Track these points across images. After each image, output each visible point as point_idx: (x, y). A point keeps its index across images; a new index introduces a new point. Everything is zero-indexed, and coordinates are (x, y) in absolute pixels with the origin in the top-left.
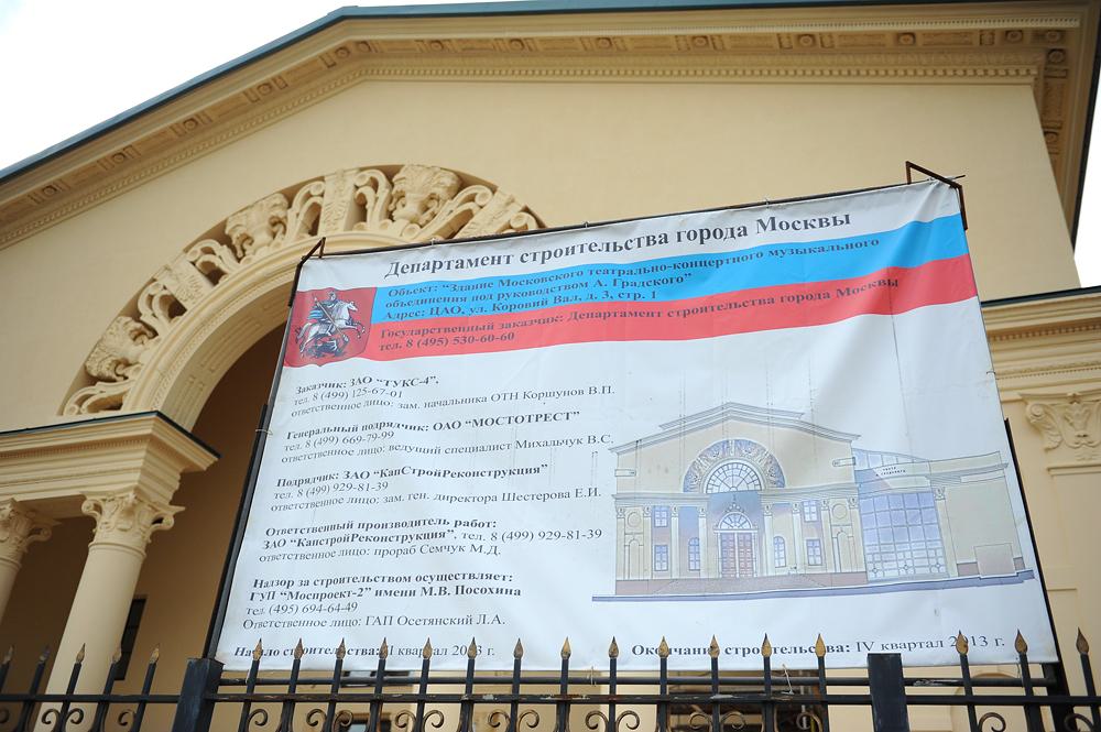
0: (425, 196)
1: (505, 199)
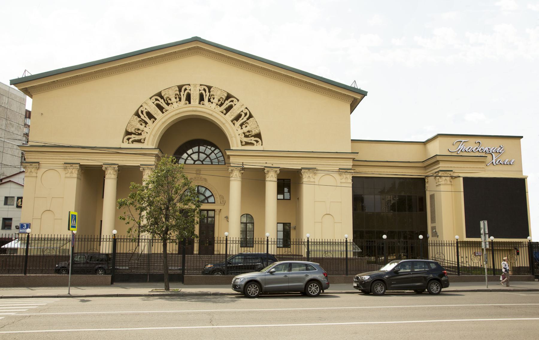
0: (219, 98)
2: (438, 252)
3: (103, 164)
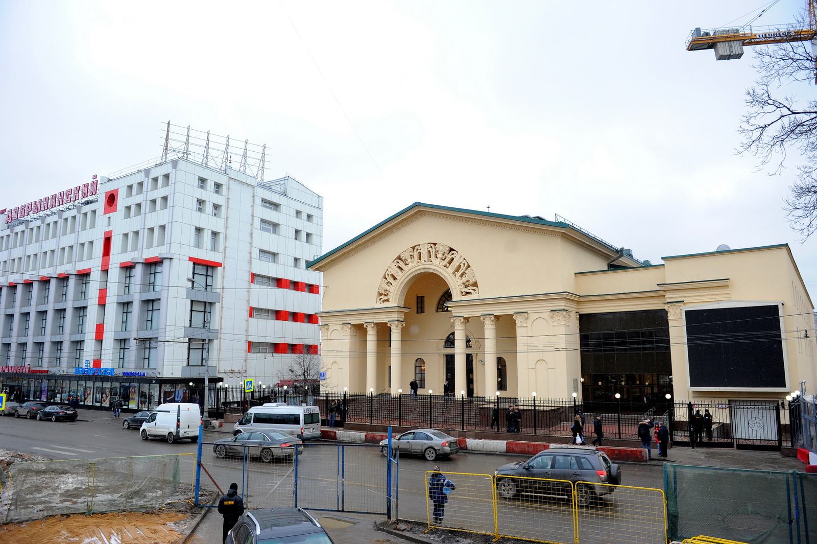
0: (443, 253)
1: (460, 256)
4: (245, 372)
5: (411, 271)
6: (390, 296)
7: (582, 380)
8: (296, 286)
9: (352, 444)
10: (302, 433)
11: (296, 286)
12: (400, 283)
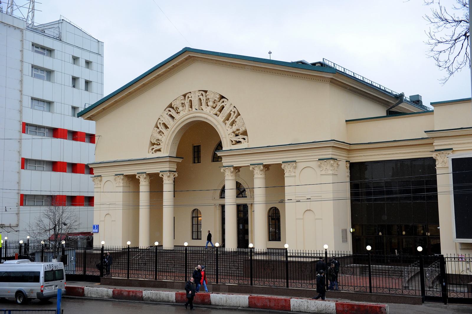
0: (213, 100)
1: (230, 104)
2: (11, 252)
3: (251, 165)
4: (17, 226)
5: (182, 120)
6: (162, 146)
7: (352, 230)
8: (75, 136)
9: (100, 299)
10: (42, 291)
11: (75, 136)
12: (171, 132)
